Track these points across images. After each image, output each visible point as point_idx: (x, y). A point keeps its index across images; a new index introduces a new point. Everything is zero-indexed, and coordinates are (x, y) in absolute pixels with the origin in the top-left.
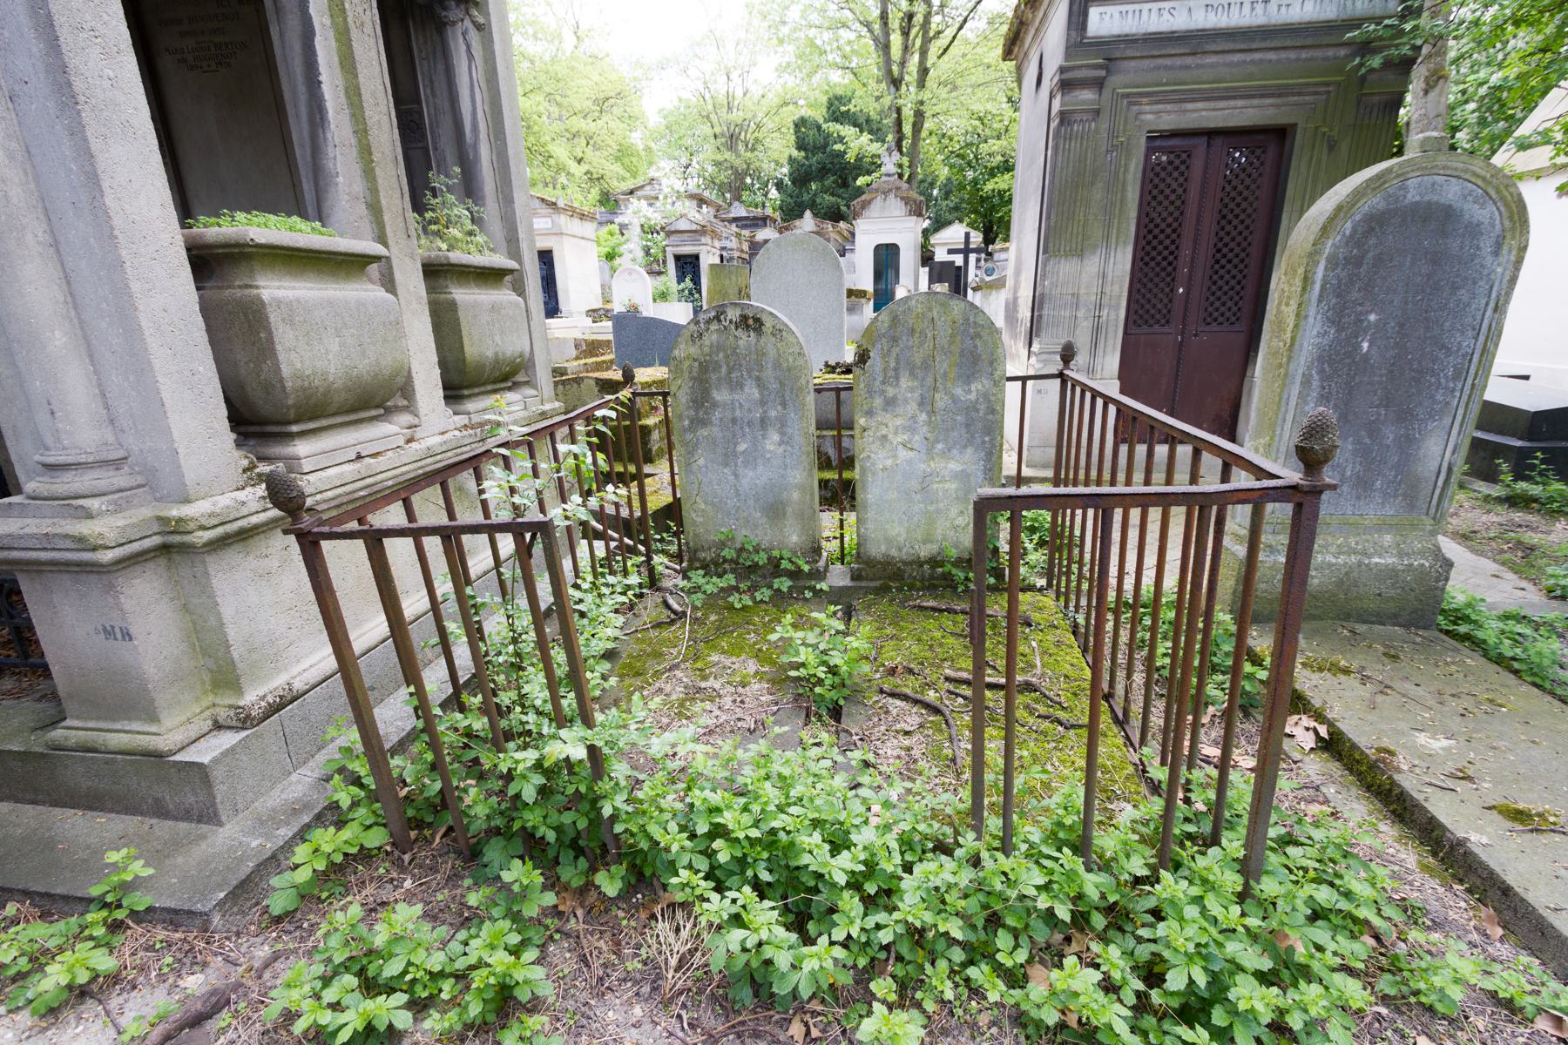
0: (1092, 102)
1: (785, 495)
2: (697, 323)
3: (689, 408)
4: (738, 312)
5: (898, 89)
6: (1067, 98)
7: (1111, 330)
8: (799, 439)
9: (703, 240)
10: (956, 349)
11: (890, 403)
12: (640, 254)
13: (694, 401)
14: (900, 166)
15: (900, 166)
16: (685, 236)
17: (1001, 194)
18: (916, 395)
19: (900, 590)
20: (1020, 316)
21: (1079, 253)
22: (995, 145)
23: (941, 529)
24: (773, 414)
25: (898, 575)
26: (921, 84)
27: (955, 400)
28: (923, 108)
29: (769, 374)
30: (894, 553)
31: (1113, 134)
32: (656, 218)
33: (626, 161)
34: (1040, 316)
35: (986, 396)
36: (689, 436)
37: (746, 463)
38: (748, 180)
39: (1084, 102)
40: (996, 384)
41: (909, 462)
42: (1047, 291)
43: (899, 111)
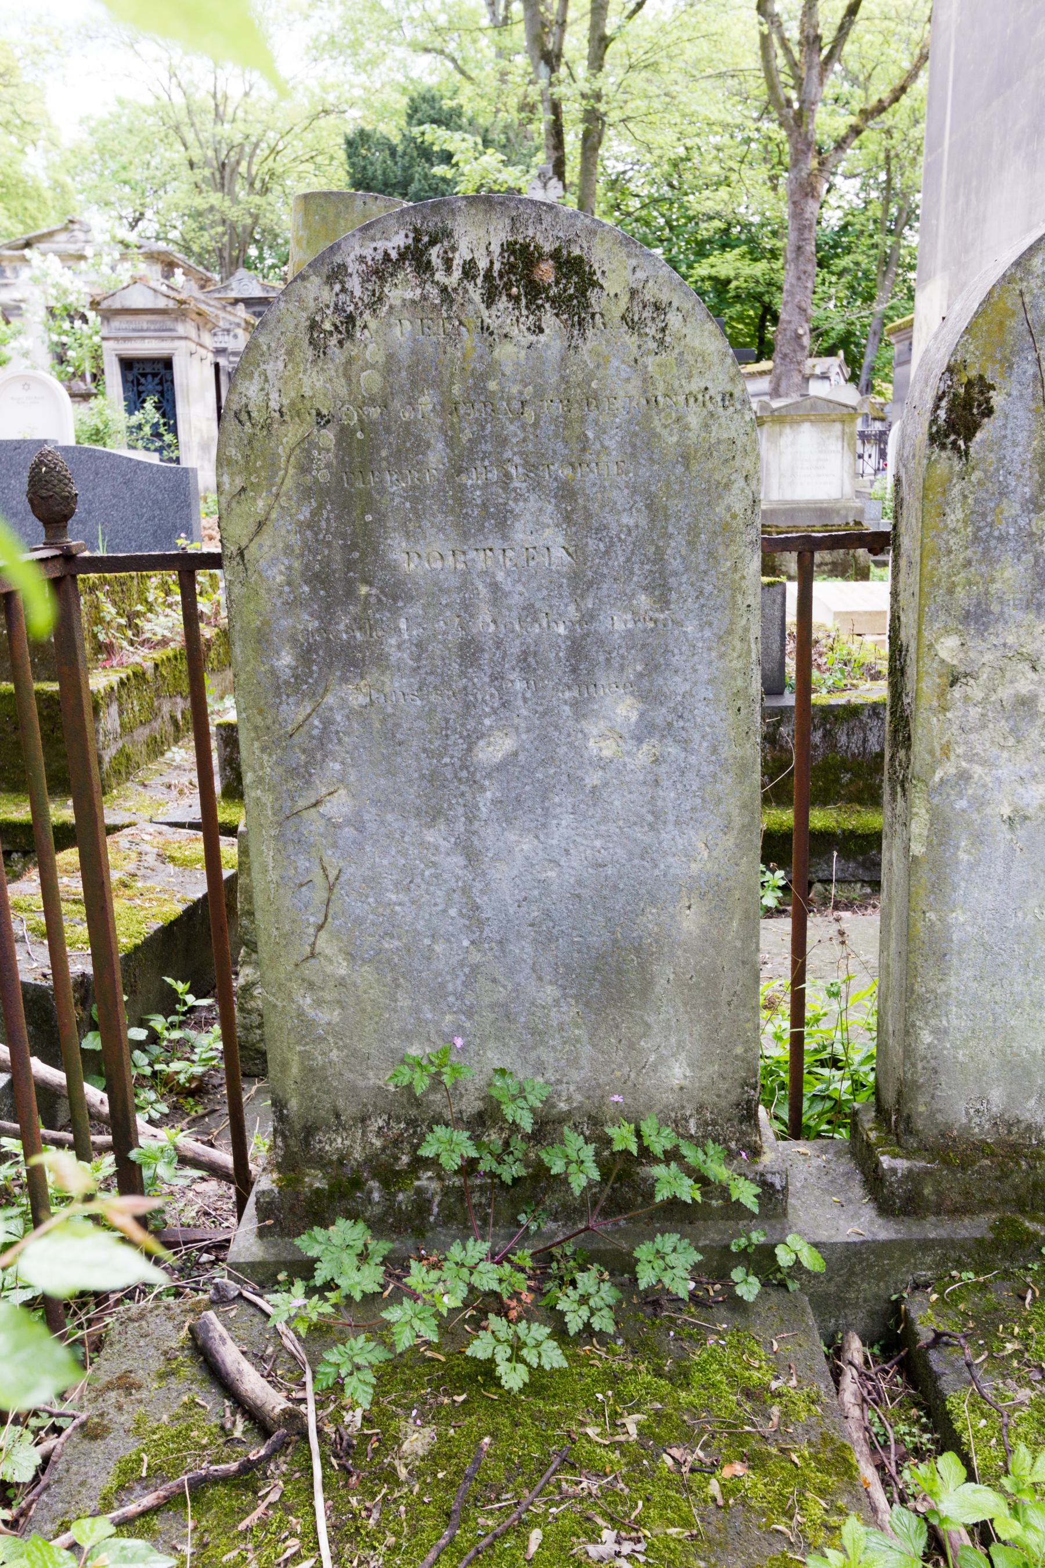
2: (337, 274)
3: (293, 605)
4: (499, 235)
5: (553, 70)
9: (181, 329)
12: (46, 359)
13: (318, 579)
16: (143, 321)
24: (618, 623)
26: (596, 62)
28: (602, 107)
29: (608, 477)
32: (78, 287)
36: (294, 711)
37: (510, 808)
38: (253, 251)
43: (556, 108)
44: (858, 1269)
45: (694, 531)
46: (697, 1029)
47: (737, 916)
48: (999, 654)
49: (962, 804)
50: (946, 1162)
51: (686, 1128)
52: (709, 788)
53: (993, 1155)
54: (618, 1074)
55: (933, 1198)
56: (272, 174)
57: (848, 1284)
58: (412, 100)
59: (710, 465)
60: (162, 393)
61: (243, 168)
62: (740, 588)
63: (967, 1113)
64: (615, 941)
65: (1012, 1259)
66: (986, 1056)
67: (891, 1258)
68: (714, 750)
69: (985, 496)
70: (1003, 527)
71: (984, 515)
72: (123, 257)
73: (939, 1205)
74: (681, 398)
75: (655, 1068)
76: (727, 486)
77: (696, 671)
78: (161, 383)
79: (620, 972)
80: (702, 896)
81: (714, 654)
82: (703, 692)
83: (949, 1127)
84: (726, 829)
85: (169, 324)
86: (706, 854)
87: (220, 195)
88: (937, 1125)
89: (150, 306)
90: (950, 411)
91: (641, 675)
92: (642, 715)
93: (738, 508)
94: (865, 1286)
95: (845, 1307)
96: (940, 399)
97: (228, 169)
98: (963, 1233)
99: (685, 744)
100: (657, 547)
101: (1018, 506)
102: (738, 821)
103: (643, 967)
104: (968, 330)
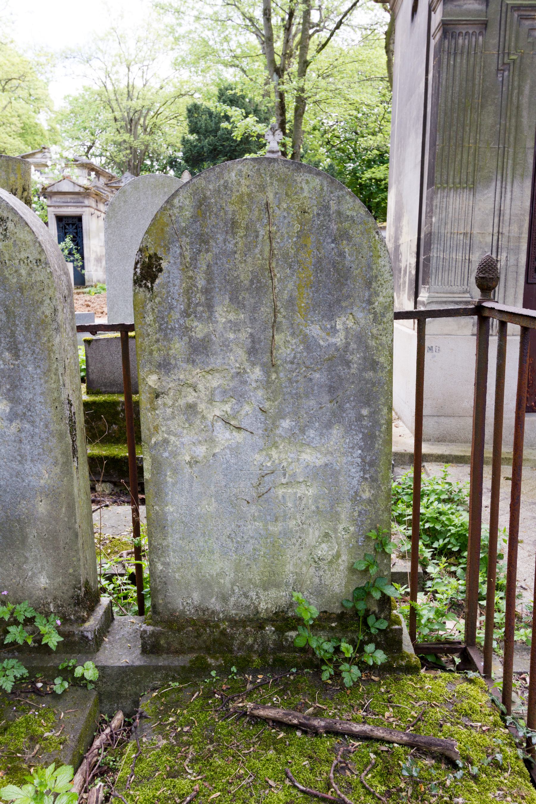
0: (478, 13)
1: (23, 506)
5: (280, 77)
6: (449, 7)
7: (510, 276)
8: (43, 411)
9: (87, 202)
10: (308, 258)
11: (199, 349)
14: (284, 145)
15: (284, 145)
16: (68, 198)
17: (378, 181)
18: (243, 336)
19: (224, 671)
20: (403, 265)
21: (471, 185)
22: (370, 141)
23: (292, 563)
25: (221, 645)
27: (309, 344)
30: (214, 604)
31: (503, 51)
33: (29, 138)
34: (428, 260)
35: (361, 339)
39: (469, 12)
40: (377, 319)
41: (236, 450)
42: (435, 229)
43: (281, 96)
44: (125, 679)
45: (28, 323)
46: (50, 560)
47: (64, 506)
48: (177, 383)
49: (166, 454)
50: (171, 629)
51: (49, 608)
52: (46, 444)
53: (195, 625)
54: (14, 581)
55: (165, 645)
56: (155, 125)
57: (121, 687)
58: (220, 90)
59: (32, 293)
60: (77, 233)
61: (141, 121)
62: (52, 350)
63: (183, 604)
64: (8, 516)
65: (199, 677)
66: (189, 577)
67: (141, 675)
68: (47, 426)
69: (162, 309)
70: (172, 324)
71: (163, 318)
72: (67, 166)
73: (168, 649)
74: (17, 261)
75: (31, 578)
76: (42, 302)
77: (35, 389)
78: (76, 228)
79: (11, 531)
80: (47, 496)
81: (42, 381)
82: (39, 399)
83: (175, 611)
84: (56, 464)
85: (81, 199)
86: (47, 476)
87: (128, 135)
88: (169, 610)
89: (71, 190)
90: (142, 269)
91: (9, 390)
92: (11, 409)
93: (48, 312)
94: (129, 688)
95: (121, 698)
96: (137, 264)
97: (134, 122)
98: (176, 663)
99: (32, 423)
100: (12, 330)
101: (179, 314)
102: (61, 460)
103: (22, 529)
104: (147, 232)
